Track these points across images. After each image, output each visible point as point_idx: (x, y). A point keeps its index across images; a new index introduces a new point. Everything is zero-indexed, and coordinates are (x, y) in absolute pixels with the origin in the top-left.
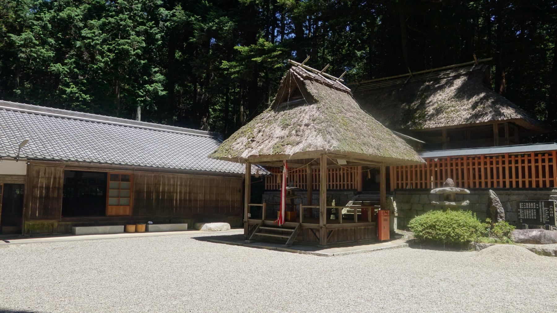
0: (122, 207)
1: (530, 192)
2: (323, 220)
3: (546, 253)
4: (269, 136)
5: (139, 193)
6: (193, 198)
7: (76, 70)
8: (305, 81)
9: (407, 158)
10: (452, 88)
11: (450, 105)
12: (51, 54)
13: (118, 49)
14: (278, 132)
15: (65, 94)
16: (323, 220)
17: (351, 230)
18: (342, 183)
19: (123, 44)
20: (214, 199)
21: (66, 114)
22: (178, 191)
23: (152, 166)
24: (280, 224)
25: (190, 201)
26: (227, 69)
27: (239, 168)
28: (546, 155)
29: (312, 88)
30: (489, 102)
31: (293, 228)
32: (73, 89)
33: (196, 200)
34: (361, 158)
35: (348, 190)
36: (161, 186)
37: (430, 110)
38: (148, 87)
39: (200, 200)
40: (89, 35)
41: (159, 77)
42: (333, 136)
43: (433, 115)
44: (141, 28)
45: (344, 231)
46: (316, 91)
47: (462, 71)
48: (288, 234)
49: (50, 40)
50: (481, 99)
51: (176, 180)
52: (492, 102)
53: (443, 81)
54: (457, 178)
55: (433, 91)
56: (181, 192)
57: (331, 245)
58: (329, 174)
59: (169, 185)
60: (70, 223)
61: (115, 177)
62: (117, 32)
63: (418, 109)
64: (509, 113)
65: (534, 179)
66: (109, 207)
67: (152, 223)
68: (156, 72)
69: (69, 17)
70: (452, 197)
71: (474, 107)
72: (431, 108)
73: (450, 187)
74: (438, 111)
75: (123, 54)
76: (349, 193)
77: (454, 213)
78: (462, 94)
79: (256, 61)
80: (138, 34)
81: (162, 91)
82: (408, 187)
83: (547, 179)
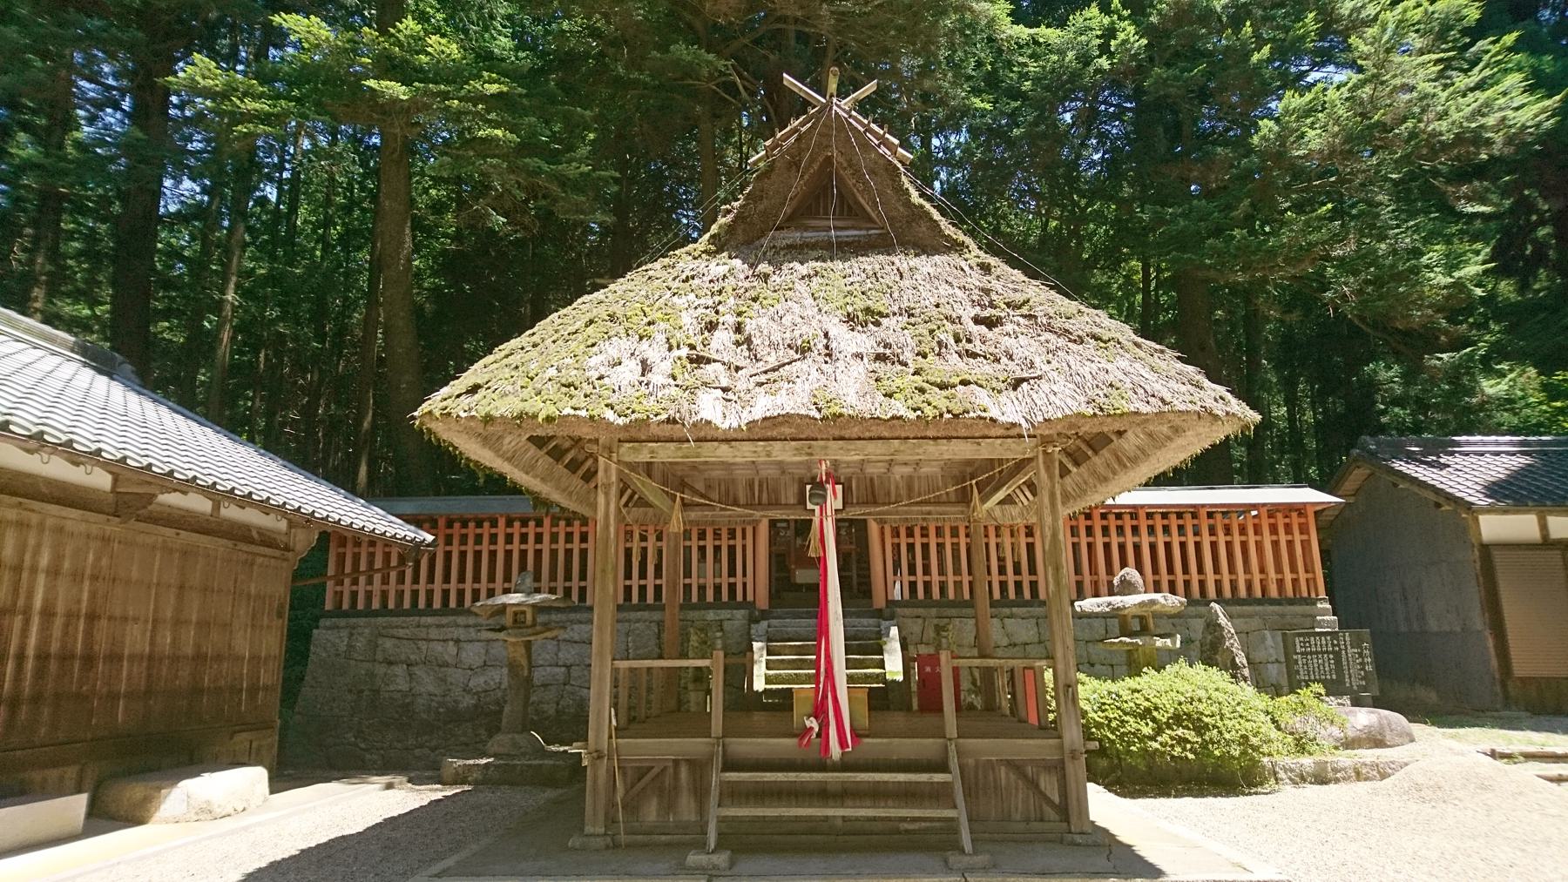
6: (102, 646)
20: (189, 650)
22: (38, 603)
24: (835, 751)
25: (89, 660)
33: (114, 658)
39: (132, 657)
48: (940, 795)
51: (32, 541)
54: (1156, 571)
56: (48, 613)
58: (628, 553)
65: (438, 586)
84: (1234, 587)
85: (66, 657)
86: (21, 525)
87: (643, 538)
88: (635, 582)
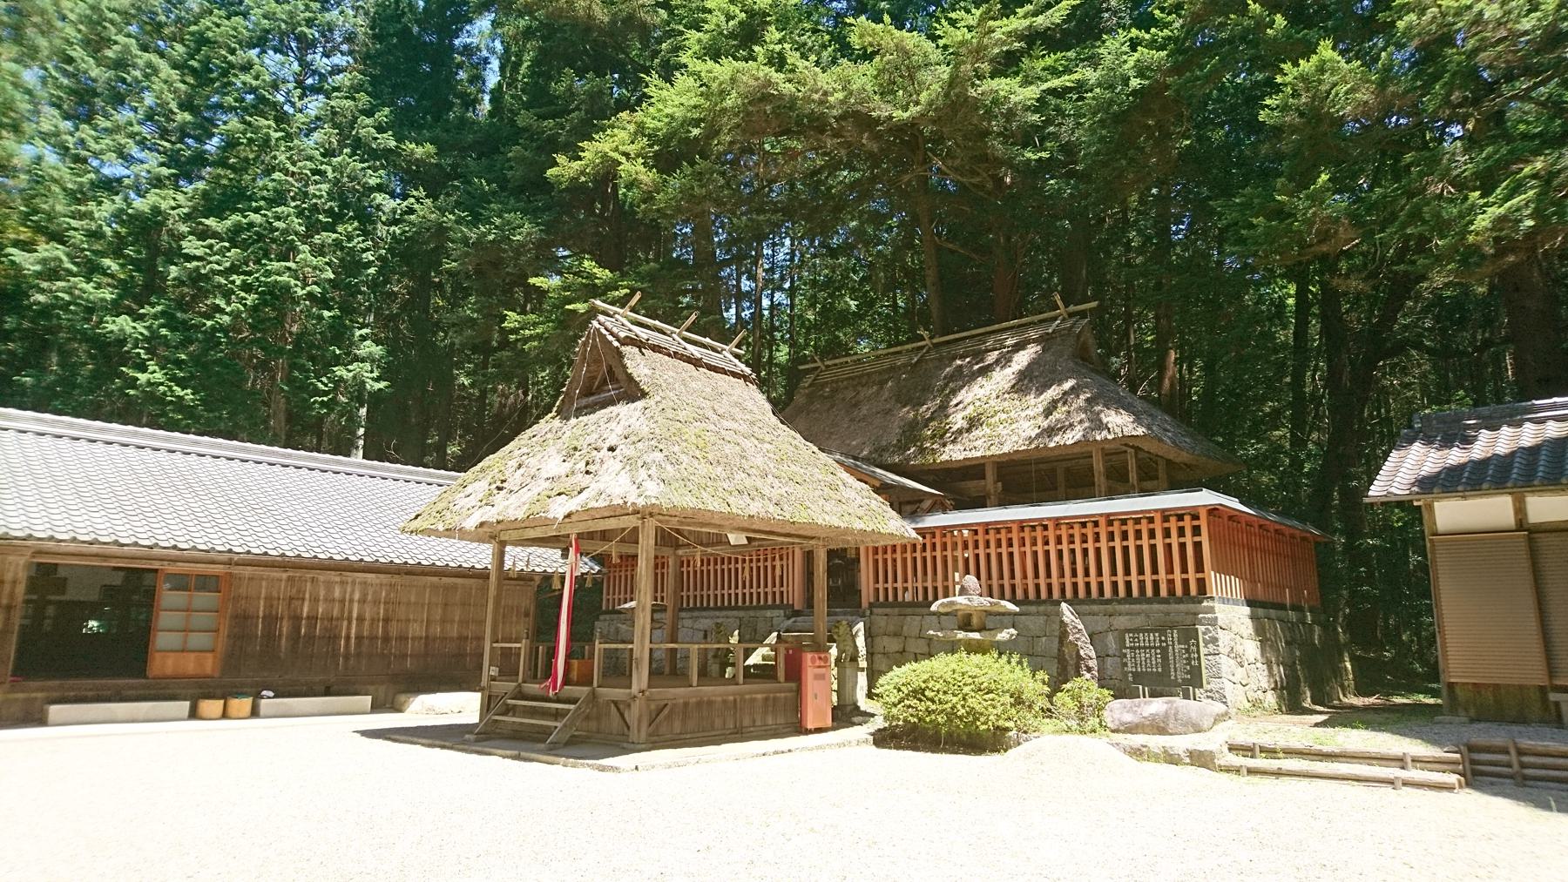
0: (192, 655)
1: (1156, 606)
2: (640, 678)
3: (1171, 759)
4: (557, 477)
5: (242, 620)
6: (394, 630)
7: (164, 331)
8: (623, 348)
9: (862, 526)
10: (1008, 371)
11: (1000, 409)
12: (108, 295)
13: (266, 284)
14: (554, 465)
15: (134, 387)
16: (640, 678)
17: (725, 702)
18: (769, 589)
19: (278, 272)
20: (455, 634)
21: (85, 429)
22: (355, 615)
23: (283, 555)
26: (514, 331)
27: (481, 556)
28: (1187, 518)
29: (638, 365)
30: (1081, 401)
31: (574, 701)
32: (154, 374)
33: (403, 638)
34: (788, 529)
35: (774, 607)
36: (306, 604)
37: (958, 420)
38: (340, 371)
40: (198, 253)
41: (369, 348)
42: (653, 471)
43: (960, 432)
44: (328, 237)
45: (704, 705)
46: (646, 371)
47: (1033, 334)
48: (557, 715)
49: (107, 262)
50: (1065, 393)
52: (1087, 400)
53: (992, 357)
54: (989, 577)
55: (964, 378)
56: (361, 619)
57: (657, 742)
59: (330, 600)
60: (39, 695)
61: (182, 583)
62: (263, 244)
63: (932, 419)
64: (1119, 423)
65: (1148, 577)
66: (157, 655)
67: (271, 694)
68: (363, 338)
69: (156, 210)
70: (975, 621)
71: (1048, 412)
72: (960, 416)
73: (969, 595)
74: (973, 423)
75: (277, 297)
76: (776, 612)
77: (977, 658)
78: (1027, 382)
79: (574, 311)
80: (319, 251)
81: (377, 380)
82: (908, 597)
83: (1192, 576)
84: (1026, 591)
85: (373, 638)
86: (342, 583)
87: (1010, 545)
88: (881, 586)
